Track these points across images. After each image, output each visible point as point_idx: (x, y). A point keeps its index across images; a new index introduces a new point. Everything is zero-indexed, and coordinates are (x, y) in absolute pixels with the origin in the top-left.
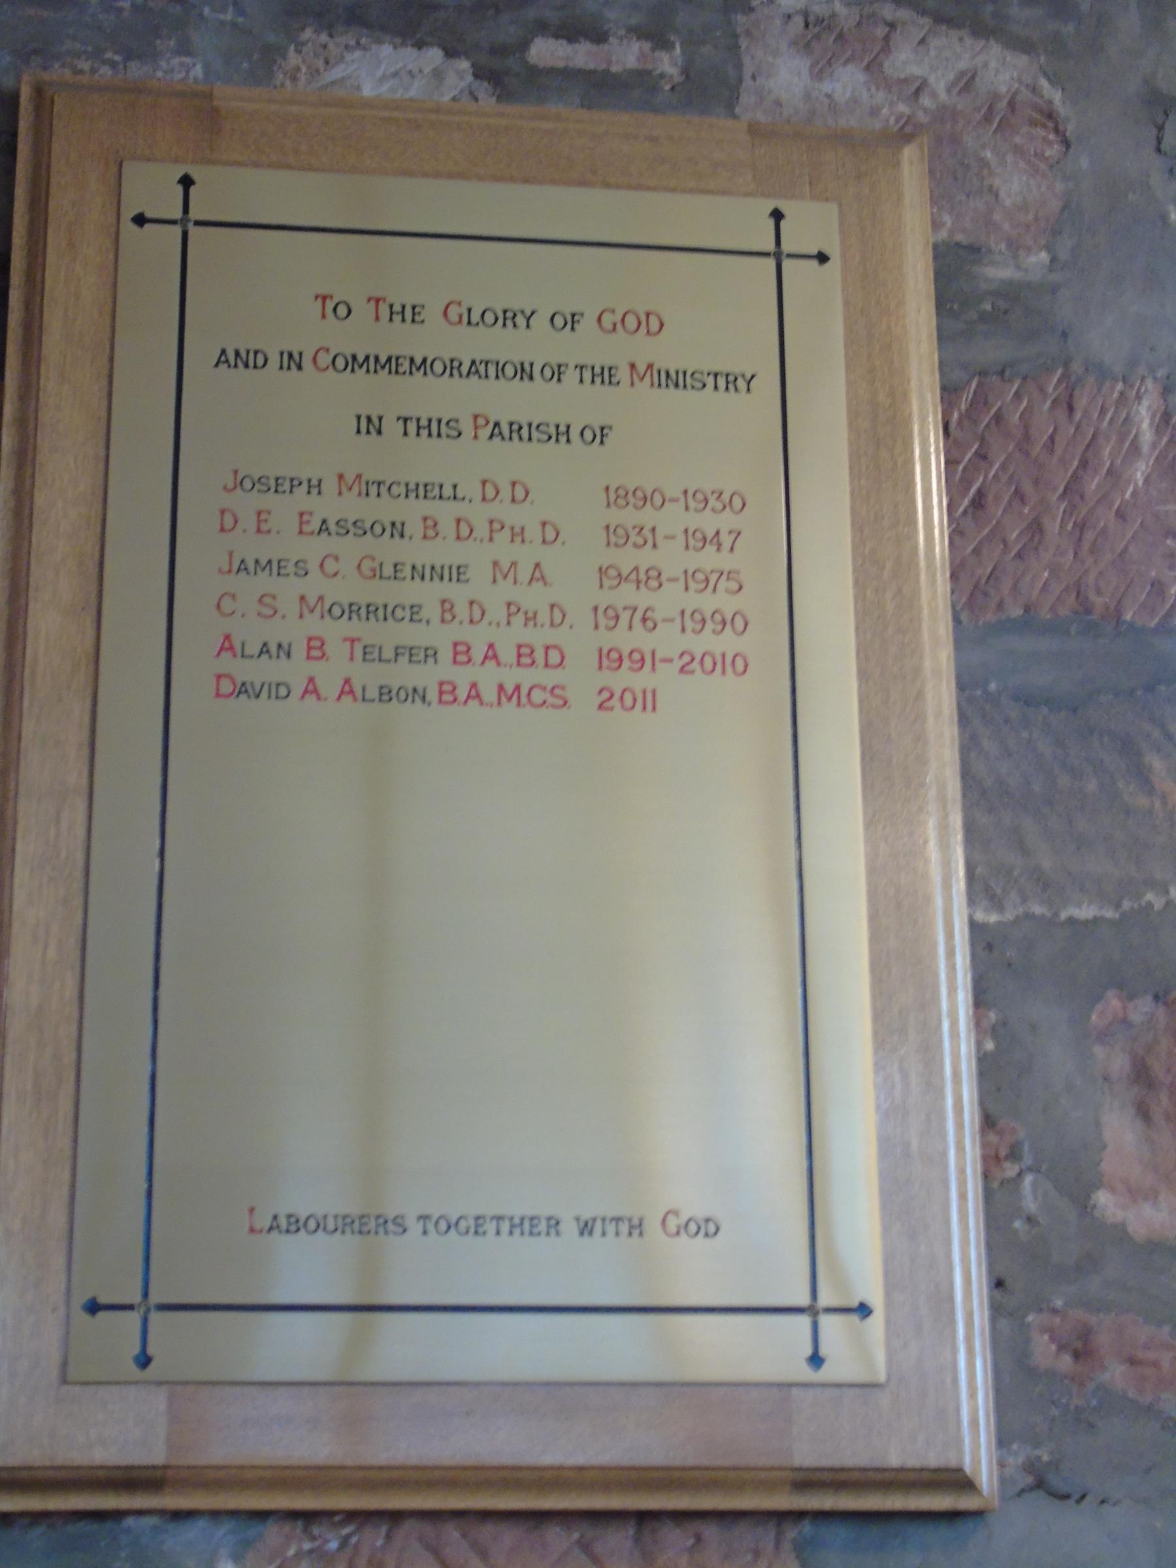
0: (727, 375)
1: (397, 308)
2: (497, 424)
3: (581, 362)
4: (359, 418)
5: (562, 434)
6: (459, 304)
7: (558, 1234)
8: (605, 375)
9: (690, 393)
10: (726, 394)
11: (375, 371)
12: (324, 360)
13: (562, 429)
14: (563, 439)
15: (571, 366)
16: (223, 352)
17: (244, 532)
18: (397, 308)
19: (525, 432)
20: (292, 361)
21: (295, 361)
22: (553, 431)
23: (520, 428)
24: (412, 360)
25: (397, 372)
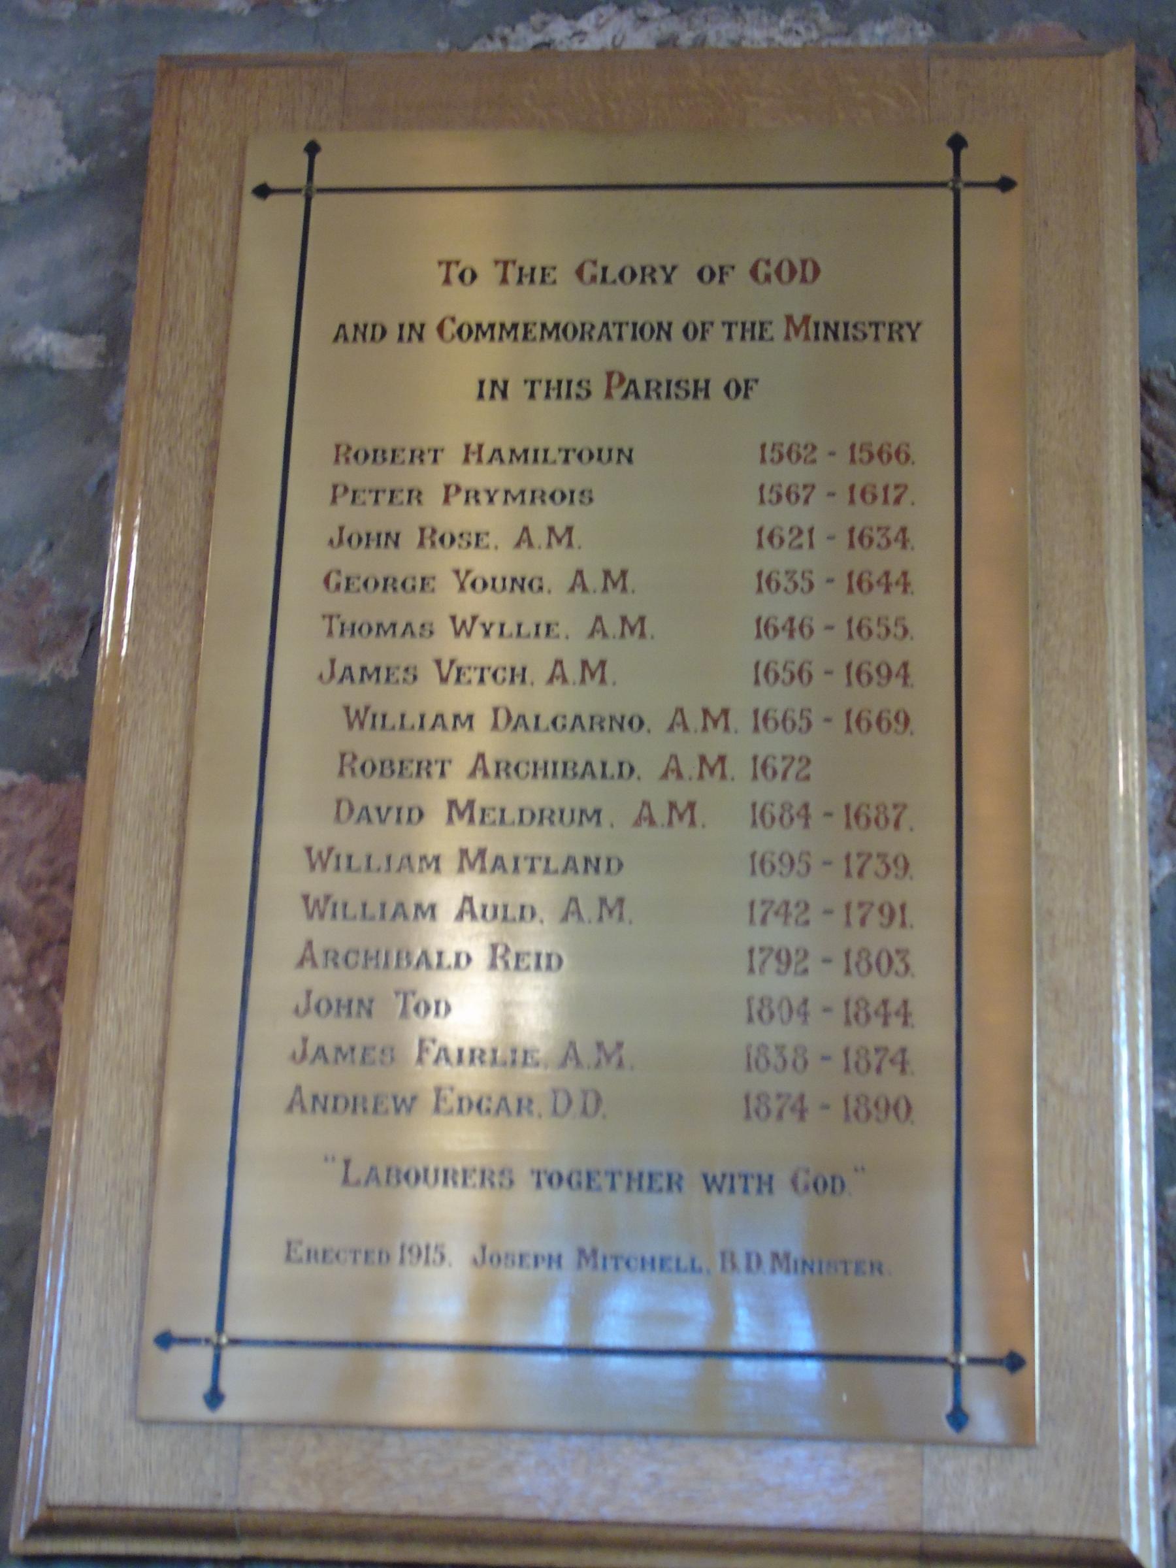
0: (891, 325)
1: (527, 270)
2: (633, 382)
3: (729, 318)
4: (482, 383)
5: (701, 389)
6: (595, 263)
7: (680, 1188)
8: (756, 331)
9: (851, 343)
10: (742, 344)
11: (501, 338)
12: (450, 329)
13: (702, 384)
14: (701, 395)
15: (718, 324)
16: (342, 326)
17: (913, 504)
18: (527, 270)
19: (663, 391)
20: (417, 332)
21: (831, 331)
22: (691, 389)
23: (659, 384)
24: (544, 326)
25: (761, 337)
